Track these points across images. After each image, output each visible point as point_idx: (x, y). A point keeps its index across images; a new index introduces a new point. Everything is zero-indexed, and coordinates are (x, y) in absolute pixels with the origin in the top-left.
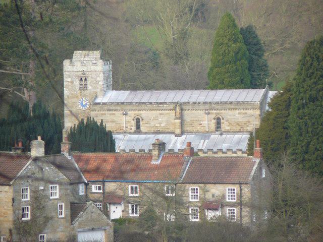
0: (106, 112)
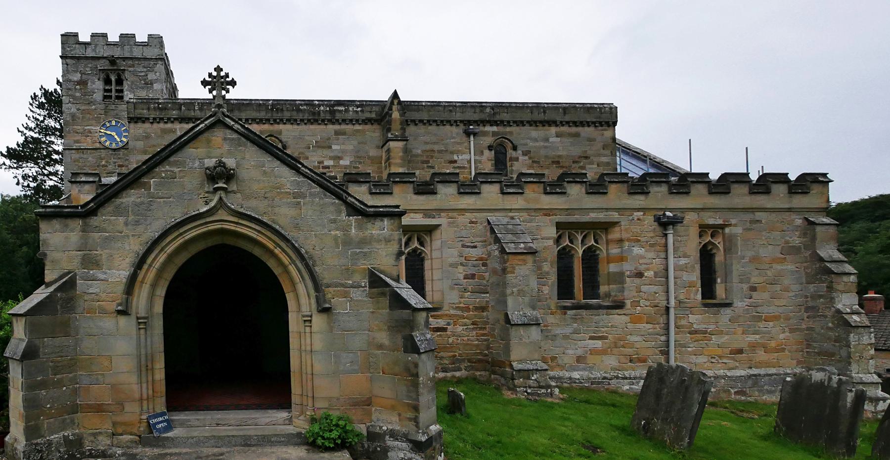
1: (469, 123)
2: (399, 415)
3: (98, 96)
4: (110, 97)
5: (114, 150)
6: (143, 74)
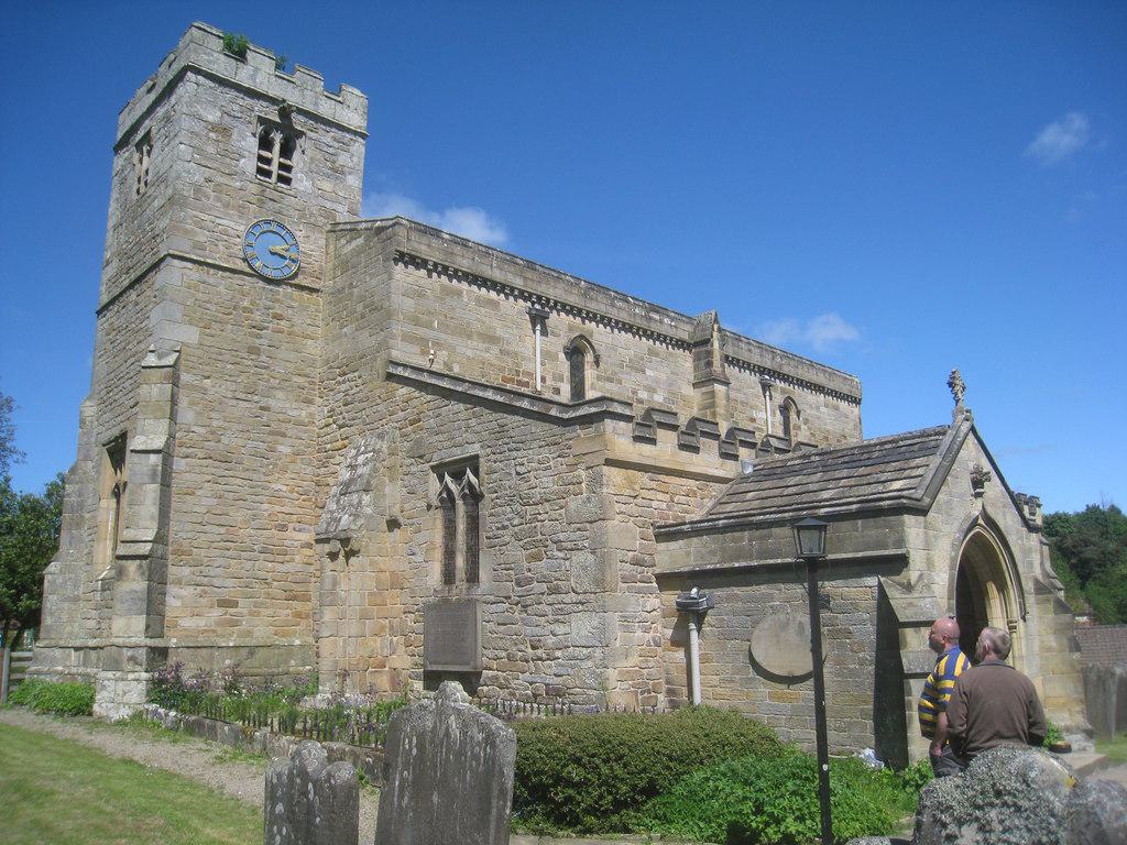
0: (464, 286)
1: (762, 371)
2: (1069, 710)
3: (249, 165)
4: (268, 174)
5: (269, 281)
6: (331, 150)
